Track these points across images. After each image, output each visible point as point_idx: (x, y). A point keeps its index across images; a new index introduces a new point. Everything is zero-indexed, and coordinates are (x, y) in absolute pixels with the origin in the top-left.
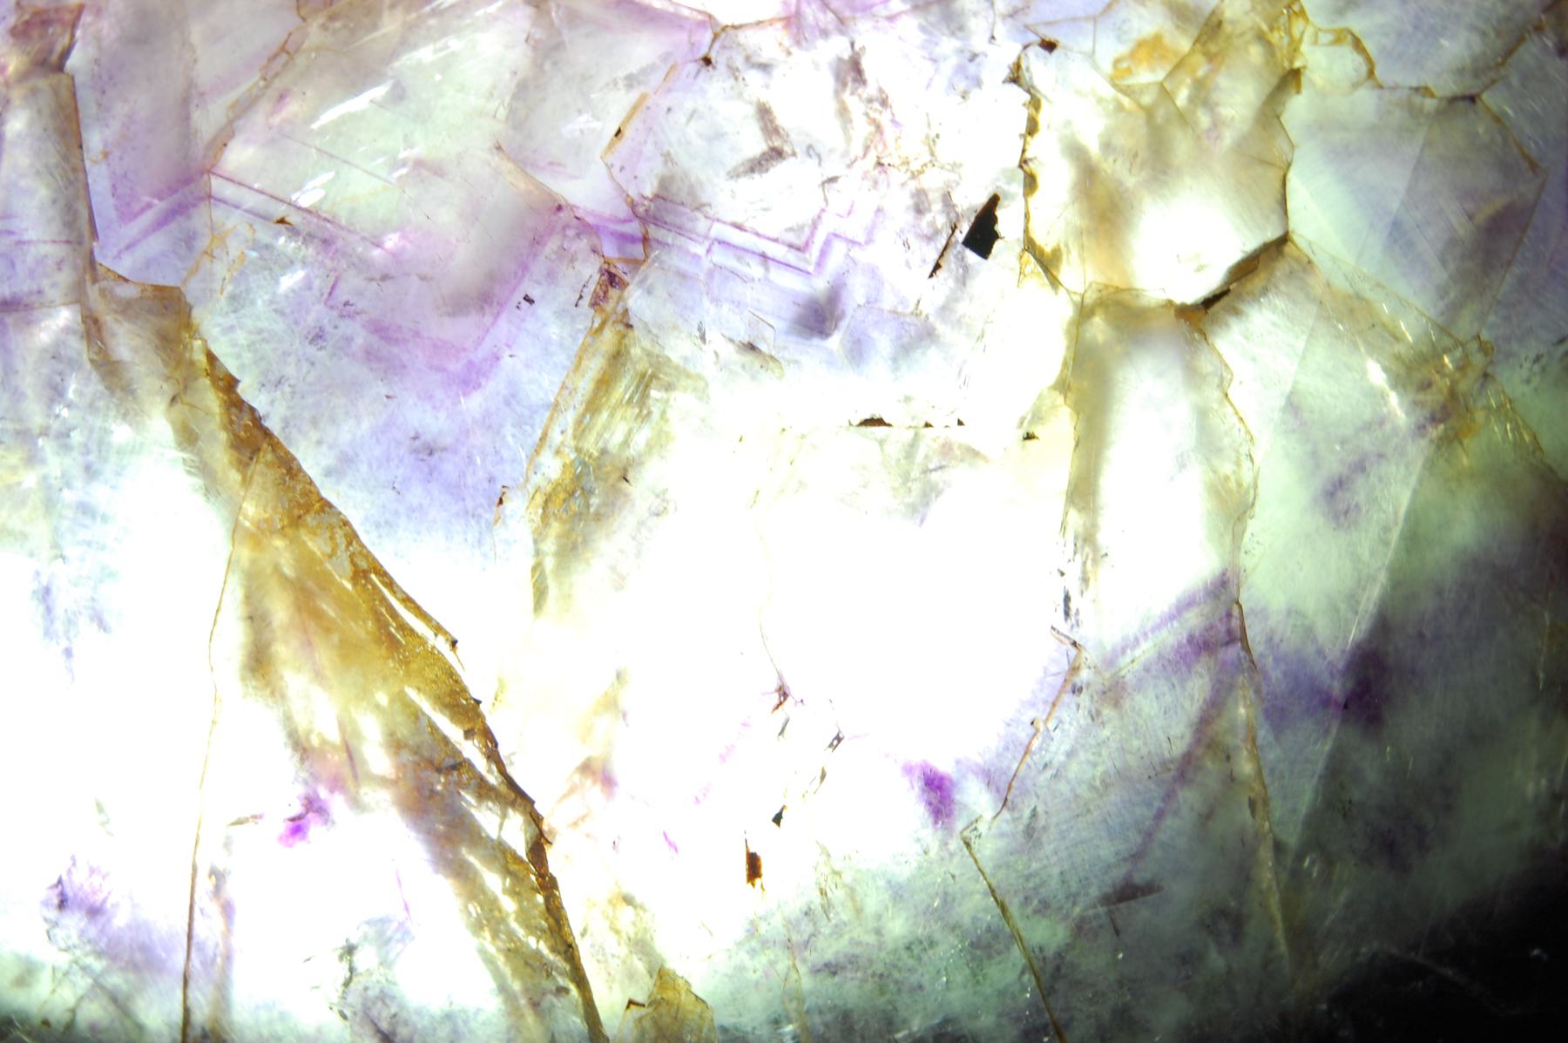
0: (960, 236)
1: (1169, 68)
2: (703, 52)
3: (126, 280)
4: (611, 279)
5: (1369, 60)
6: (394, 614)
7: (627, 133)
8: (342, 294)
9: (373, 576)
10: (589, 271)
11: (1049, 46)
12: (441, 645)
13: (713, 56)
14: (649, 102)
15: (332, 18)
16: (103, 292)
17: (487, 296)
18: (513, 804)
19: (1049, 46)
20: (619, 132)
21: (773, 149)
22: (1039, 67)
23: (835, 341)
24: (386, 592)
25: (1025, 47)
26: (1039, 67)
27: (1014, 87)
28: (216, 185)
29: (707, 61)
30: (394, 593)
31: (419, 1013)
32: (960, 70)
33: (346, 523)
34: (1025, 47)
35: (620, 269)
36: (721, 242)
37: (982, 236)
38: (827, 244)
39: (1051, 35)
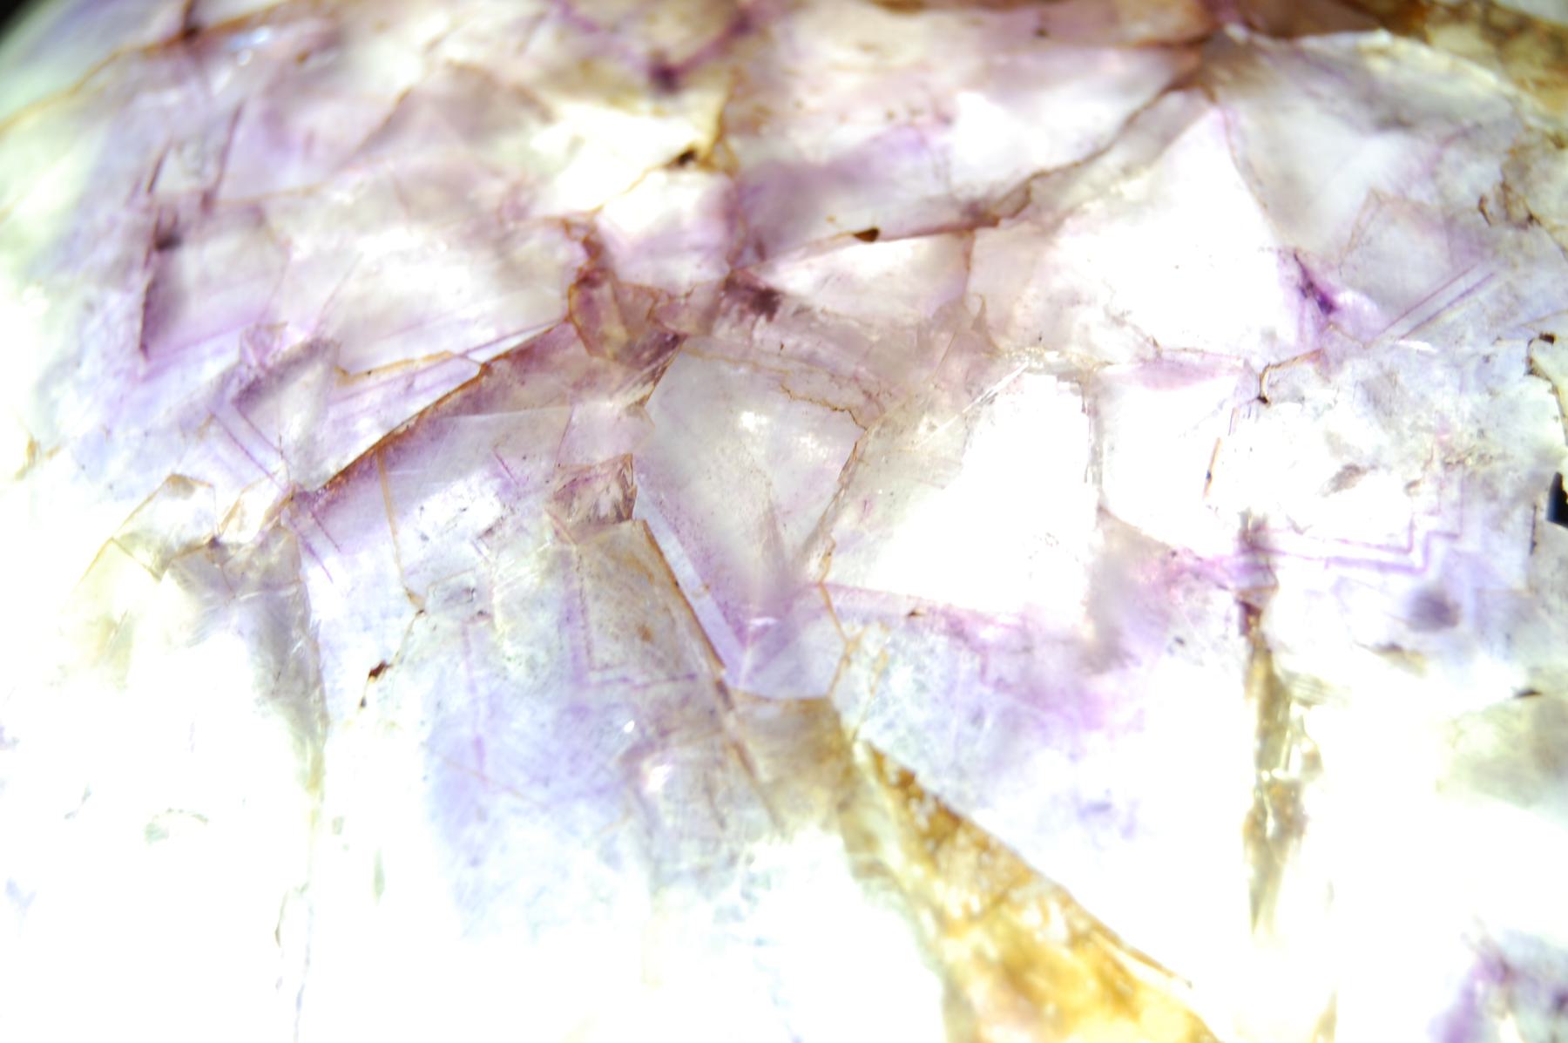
2: (1254, 394)
4: (1250, 611)
8: (992, 675)
10: (1225, 605)
11: (1550, 339)
13: (1266, 392)
15: (884, 425)
16: (741, 719)
17: (1107, 654)
19: (1550, 339)
22: (1543, 357)
23: (1465, 627)
25: (1530, 342)
26: (1543, 357)
27: (1533, 378)
29: (1263, 400)
32: (1479, 372)
34: (1530, 342)
39: (1548, 330)
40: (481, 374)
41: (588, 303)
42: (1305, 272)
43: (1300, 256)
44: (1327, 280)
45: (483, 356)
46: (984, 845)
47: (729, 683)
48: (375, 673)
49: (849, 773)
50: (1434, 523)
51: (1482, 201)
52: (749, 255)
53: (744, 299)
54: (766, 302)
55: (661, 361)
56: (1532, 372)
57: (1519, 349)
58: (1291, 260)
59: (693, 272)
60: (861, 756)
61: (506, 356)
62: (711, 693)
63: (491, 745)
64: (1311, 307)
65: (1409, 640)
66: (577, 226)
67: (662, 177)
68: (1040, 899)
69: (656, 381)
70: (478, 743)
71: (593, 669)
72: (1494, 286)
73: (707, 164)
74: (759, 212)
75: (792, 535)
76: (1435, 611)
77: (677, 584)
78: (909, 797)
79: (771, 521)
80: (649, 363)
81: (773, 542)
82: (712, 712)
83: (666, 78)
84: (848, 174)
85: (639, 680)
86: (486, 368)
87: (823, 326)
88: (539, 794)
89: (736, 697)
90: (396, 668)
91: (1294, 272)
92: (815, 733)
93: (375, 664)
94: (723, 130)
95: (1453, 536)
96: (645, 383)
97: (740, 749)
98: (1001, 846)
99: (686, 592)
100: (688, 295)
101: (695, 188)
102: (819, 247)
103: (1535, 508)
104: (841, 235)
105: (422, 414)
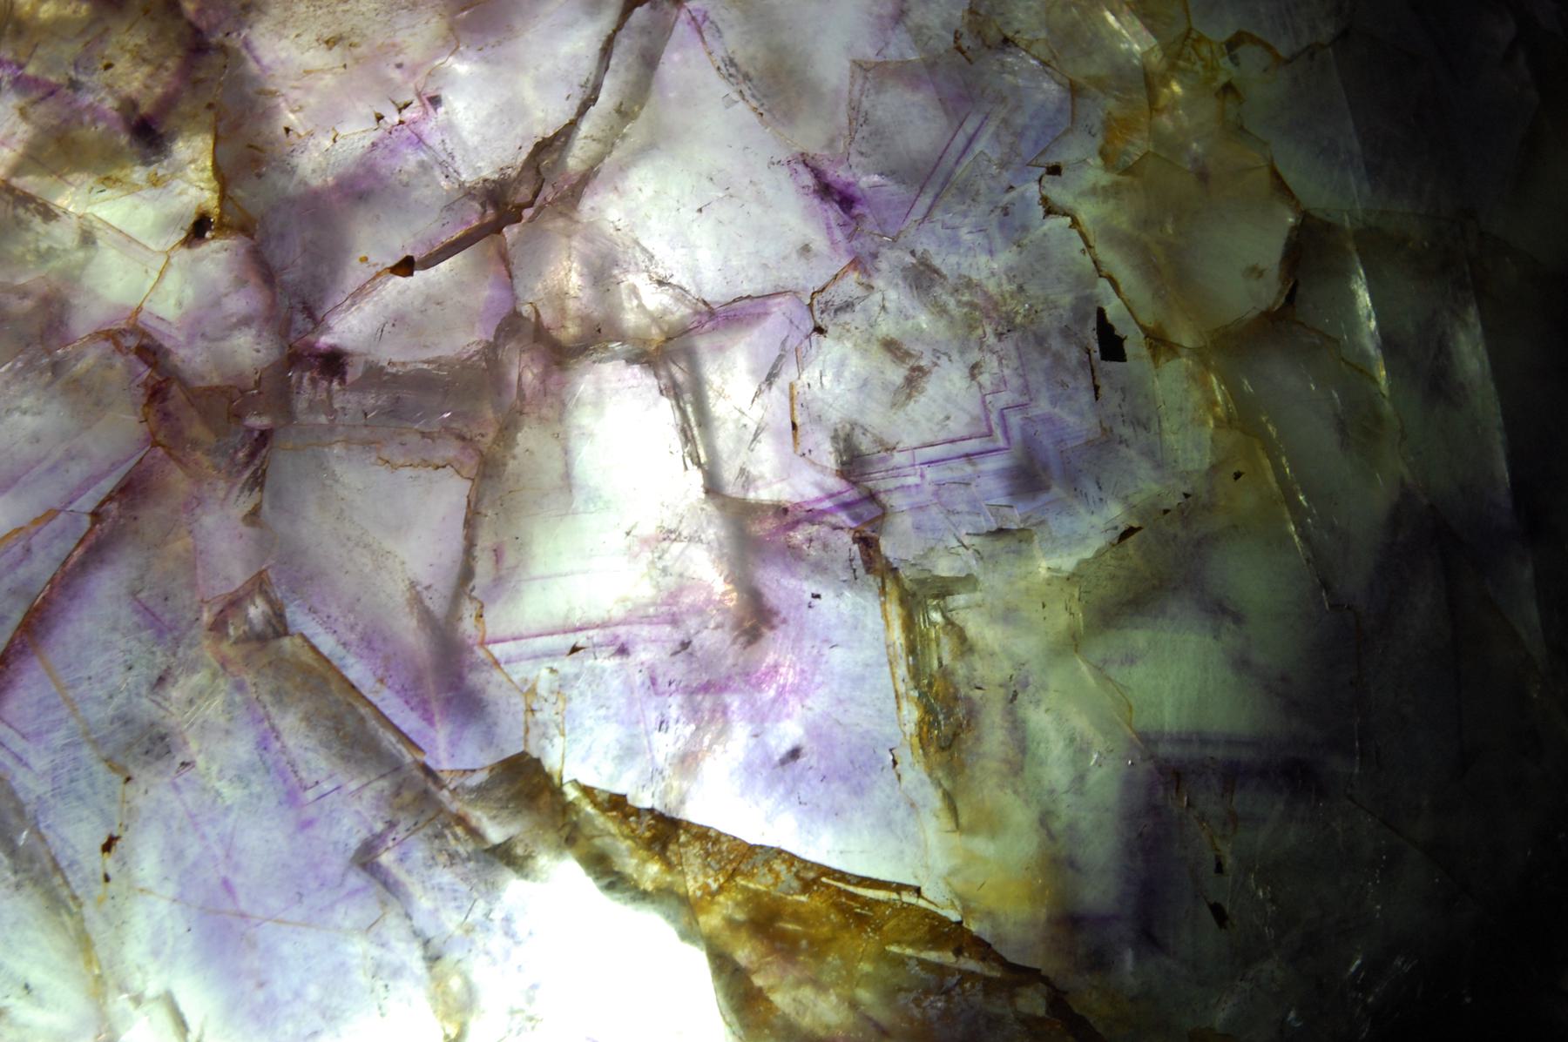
0: (1097, 355)
1: (954, 178)
2: (810, 326)
3: (474, 771)
4: (867, 544)
5: (1268, 48)
6: (854, 897)
7: (798, 421)
9: (824, 879)
11: (1055, 170)
12: (907, 898)
14: (798, 388)
18: (1021, 984)
20: (794, 426)
21: (913, 369)
24: (860, 891)
28: (497, 650)
30: (848, 883)
31: (30, 897)
33: (780, 852)
34: (1040, 181)
35: (868, 532)
36: (930, 463)
37: (1112, 346)
38: (1003, 417)
39: (1052, 161)
40: (93, 524)
41: (166, 416)
42: (818, 174)
43: (808, 160)
44: (839, 174)
45: (87, 503)
46: (703, 835)
47: (431, 763)
48: (107, 848)
49: (567, 808)
50: (1005, 398)
51: (957, 36)
52: (300, 320)
53: (311, 368)
54: (334, 363)
55: (257, 462)
56: (1050, 210)
57: (1033, 190)
58: (800, 168)
59: (249, 350)
60: (572, 794)
61: (110, 498)
62: (420, 775)
63: (238, 880)
64: (833, 212)
65: (1014, 519)
66: (123, 332)
67: (185, 254)
68: (767, 862)
69: (262, 486)
70: (226, 884)
71: (306, 789)
72: (991, 128)
73: (223, 228)
74: (276, 231)
75: (437, 605)
76: (1027, 479)
77: (353, 687)
78: (626, 816)
79: (416, 599)
80: (247, 465)
81: (426, 616)
82: (426, 792)
83: (148, 134)
84: (362, 188)
85: (353, 786)
86: (96, 515)
87: (394, 375)
88: (297, 913)
89: (445, 777)
90: (125, 836)
91: (808, 179)
92: (525, 782)
93: (104, 840)
94: (223, 177)
95: (1021, 407)
96: (252, 490)
97: (461, 820)
98: (720, 834)
99: (365, 691)
100: (258, 383)
101: (218, 256)
102: (360, 293)
103: (1088, 352)
104: (378, 274)
105: (52, 580)
